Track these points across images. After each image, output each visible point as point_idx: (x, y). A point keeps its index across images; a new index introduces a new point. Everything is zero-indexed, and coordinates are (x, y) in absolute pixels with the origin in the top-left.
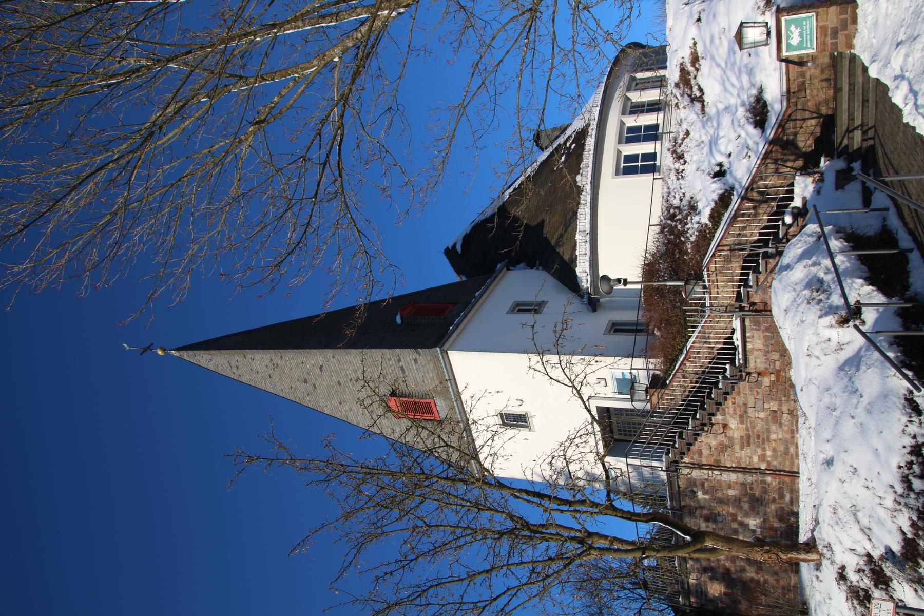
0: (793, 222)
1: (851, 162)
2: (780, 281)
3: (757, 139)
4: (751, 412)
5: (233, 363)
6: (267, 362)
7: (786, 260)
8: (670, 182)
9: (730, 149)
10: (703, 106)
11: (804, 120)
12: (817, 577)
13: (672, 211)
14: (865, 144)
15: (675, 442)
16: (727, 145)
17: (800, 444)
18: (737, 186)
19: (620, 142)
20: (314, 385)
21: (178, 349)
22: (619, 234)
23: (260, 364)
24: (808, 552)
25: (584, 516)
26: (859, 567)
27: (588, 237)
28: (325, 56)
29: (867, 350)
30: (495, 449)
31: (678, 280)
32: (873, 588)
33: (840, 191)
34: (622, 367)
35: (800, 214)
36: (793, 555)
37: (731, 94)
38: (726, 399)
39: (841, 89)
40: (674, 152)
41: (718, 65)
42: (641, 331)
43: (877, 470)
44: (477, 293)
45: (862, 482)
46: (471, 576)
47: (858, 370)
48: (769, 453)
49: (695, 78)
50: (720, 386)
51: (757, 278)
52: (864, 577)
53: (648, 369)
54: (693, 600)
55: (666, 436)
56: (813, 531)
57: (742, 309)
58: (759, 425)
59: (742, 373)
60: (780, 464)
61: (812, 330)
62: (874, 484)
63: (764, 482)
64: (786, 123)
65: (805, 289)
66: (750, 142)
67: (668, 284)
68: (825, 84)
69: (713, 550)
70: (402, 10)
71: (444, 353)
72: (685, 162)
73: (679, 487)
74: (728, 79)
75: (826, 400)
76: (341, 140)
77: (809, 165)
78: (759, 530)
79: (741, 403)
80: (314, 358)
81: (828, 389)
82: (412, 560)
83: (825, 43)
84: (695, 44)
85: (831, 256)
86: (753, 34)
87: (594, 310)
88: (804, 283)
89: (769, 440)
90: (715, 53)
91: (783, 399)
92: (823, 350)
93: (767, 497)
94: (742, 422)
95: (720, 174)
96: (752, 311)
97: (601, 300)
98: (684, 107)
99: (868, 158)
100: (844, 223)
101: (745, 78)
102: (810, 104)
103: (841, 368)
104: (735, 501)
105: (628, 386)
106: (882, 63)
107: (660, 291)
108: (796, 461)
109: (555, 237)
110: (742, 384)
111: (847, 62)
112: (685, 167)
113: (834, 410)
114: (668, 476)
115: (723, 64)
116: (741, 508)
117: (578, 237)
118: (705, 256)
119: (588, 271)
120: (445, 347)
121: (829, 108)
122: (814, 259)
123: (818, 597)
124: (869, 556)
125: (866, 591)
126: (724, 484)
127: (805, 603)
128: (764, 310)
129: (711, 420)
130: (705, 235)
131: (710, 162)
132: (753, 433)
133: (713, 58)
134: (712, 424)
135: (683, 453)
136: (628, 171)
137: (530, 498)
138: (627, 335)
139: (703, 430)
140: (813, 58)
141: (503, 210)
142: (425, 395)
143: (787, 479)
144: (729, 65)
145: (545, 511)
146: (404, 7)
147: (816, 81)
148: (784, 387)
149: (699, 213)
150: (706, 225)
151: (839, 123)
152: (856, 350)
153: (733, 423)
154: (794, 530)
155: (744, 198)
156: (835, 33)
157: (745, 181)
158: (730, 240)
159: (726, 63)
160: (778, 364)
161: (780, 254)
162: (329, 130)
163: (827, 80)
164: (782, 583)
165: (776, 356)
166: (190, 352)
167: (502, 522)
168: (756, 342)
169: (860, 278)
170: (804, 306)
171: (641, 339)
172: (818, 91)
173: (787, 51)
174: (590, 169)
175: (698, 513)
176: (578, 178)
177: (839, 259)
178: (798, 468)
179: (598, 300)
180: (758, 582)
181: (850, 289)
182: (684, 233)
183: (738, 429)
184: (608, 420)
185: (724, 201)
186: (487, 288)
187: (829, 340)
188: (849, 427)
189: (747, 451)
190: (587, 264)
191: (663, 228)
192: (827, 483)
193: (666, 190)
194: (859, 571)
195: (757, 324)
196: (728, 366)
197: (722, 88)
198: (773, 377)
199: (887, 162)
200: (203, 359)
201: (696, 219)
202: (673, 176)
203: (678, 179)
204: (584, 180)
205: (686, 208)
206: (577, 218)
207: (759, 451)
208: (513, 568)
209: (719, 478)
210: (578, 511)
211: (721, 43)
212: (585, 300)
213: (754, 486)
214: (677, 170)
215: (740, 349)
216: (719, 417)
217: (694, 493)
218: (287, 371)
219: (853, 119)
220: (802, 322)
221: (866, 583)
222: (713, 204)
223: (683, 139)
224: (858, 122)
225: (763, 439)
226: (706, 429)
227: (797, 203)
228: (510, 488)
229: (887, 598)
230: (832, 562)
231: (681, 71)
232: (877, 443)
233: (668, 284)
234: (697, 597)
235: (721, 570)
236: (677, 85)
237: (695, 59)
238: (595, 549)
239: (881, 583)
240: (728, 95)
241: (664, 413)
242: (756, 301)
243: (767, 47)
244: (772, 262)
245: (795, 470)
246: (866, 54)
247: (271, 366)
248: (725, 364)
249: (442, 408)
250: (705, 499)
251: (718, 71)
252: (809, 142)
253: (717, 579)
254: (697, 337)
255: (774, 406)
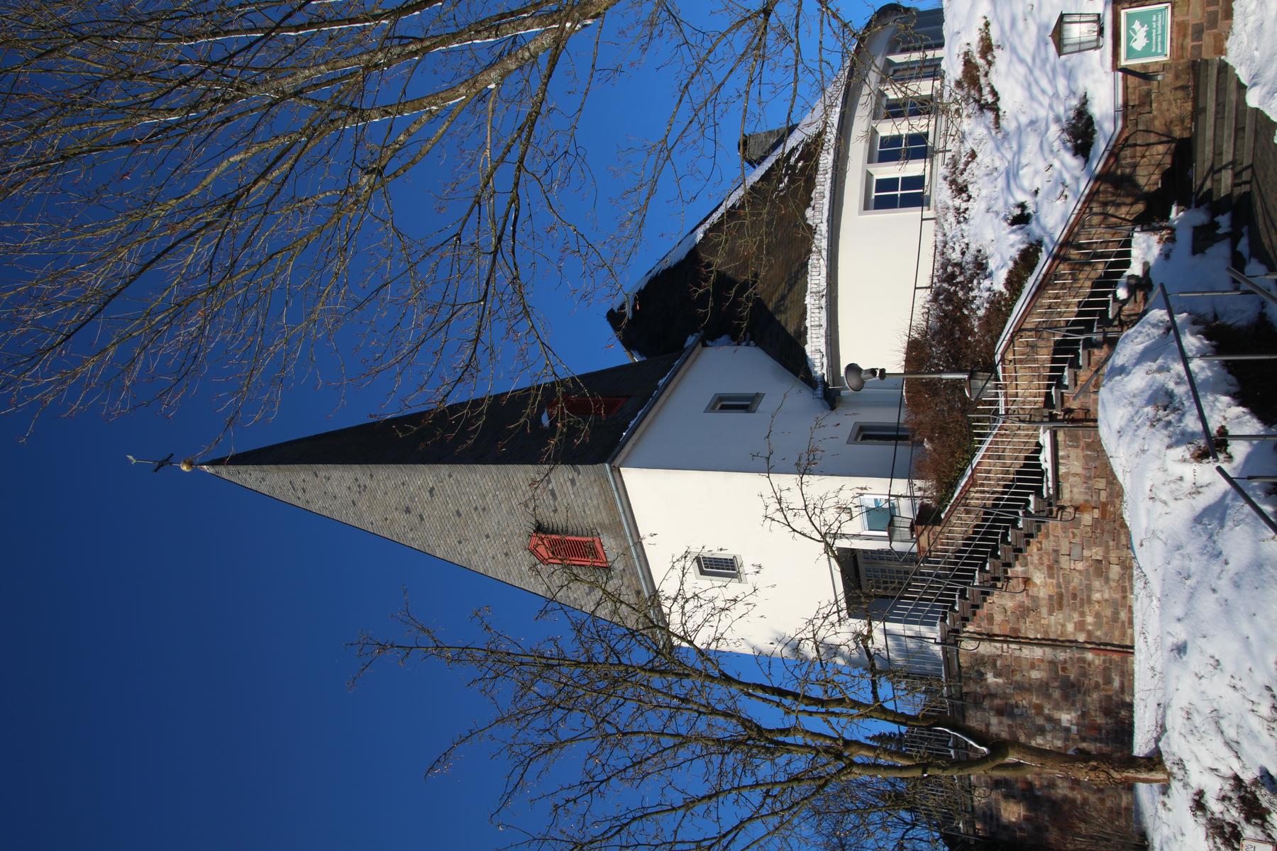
0: (1129, 298)
1: (1217, 215)
2: (1111, 390)
3: (1078, 173)
4: (1065, 562)
5: (298, 484)
6: (349, 482)
7: (1120, 358)
8: (946, 226)
9: (1038, 183)
10: (997, 117)
11: (1148, 145)
12: (1164, 804)
13: (950, 269)
14: (1237, 191)
15: (954, 603)
16: (1029, 179)
17: (1137, 607)
18: (1046, 240)
19: (870, 161)
20: (421, 516)
21: (213, 463)
22: (872, 296)
23: (339, 484)
24: (1151, 770)
25: (843, 720)
26: (1223, 793)
27: (824, 300)
28: (476, 81)
29: (1234, 499)
30: (720, 631)
31: (960, 371)
32: (1243, 823)
33: (1198, 256)
34: (878, 489)
35: (1141, 285)
36: (1131, 774)
37: (1041, 104)
38: (1028, 543)
39: (1204, 110)
40: (953, 182)
41: (1022, 61)
42: (905, 438)
43: (1249, 665)
44: (661, 382)
45: (1227, 679)
46: (689, 804)
47: (1222, 527)
48: (1090, 619)
49: (986, 75)
50: (1020, 525)
51: (1076, 375)
52: (1230, 807)
53: (912, 497)
54: (978, 826)
55: (942, 595)
56: (1157, 740)
57: (1052, 418)
58: (1076, 581)
59: (1052, 506)
60: (1106, 634)
61: (1157, 464)
62: (1244, 684)
63: (1083, 660)
64: (1121, 150)
65: (1147, 404)
66: (1067, 177)
67: (945, 376)
68: (1180, 94)
69: (1017, 766)
70: (589, 22)
71: (616, 470)
72: (970, 197)
73: (959, 666)
74: (1037, 82)
75: (1177, 563)
76: (516, 217)
77: (1152, 218)
78: (1074, 728)
79: (1050, 549)
80: (421, 478)
81: (1179, 548)
82: (602, 782)
83: (1182, 47)
84: (987, 25)
85: (1185, 360)
86: (1077, 32)
87: (833, 408)
88: (1146, 396)
89: (1089, 601)
90: (1016, 42)
91: (1111, 543)
92: (1172, 492)
93: (1086, 682)
94: (1051, 576)
95: (1021, 219)
96: (1069, 421)
97: (843, 393)
98: (969, 116)
99: (1241, 209)
100: (1204, 309)
101: (1062, 84)
102: (1157, 123)
103: (1198, 519)
104: (1041, 686)
105: (883, 517)
106: (1266, 89)
107: (932, 387)
108: (1129, 631)
109: (774, 300)
110: (1051, 523)
111: (1215, 71)
112: (969, 204)
113: (1188, 577)
114: (944, 651)
115: (1029, 60)
116: (1049, 696)
117: (809, 300)
118: (998, 337)
119: (823, 349)
120: (616, 463)
121: (1185, 129)
122: (1160, 361)
123: (1165, 831)
124: (1236, 778)
125: (1234, 826)
126: (1024, 662)
127: (1143, 835)
128: (1086, 421)
129: (1006, 572)
130: (1000, 308)
131: (1006, 203)
132: (1067, 590)
133: (1014, 50)
134: (1009, 578)
135: (965, 620)
136: (883, 204)
137: (767, 696)
138: (880, 444)
139: (994, 586)
140: (1164, 66)
141: (694, 254)
142: (591, 532)
143: (1116, 657)
144: (1038, 62)
145: (787, 713)
146: (593, 17)
147: (1166, 90)
148: (1111, 526)
149: (991, 275)
150: (1001, 293)
151: (1199, 158)
152: (1220, 495)
153: (1038, 578)
154: (1124, 731)
155: (1056, 258)
156: (1198, 32)
157: (1059, 233)
158: (1034, 320)
159: (1034, 59)
160: (1103, 495)
161: (1112, 343)
162: (496, 205)
163: (1183, 88)
164: (1109, 803)
165: (1101, 484)
166: (232, 468)
167: (726, 728)
168: (1073, 464)
169: (1226, 394)
170: (1145, 430)
171: (904, 450)
172: (1170, 104)
173: (1127, 58)
174: (826, 201)
175: (986, 704)
176: (809, 213)
177: (1195, 365)
178: (1132, 640)
179: (838, 392)
180: (1073, 801)
181: (1212, 410)
182: (967, 302)
183: (1045, 585)
184: (852, 565)
185: (1027, 260)
186: (676, 373)
187: (1181, 479)
188: (1207, 605)
189: (1059, 617)
190: (823, 340)
191: (936, 295)
192: (1178, 678)
193: (940, 238)
194: (1224, 799)
195: (1074, 438)
196: (1031, 498)
197: (1027, 94)
198: (1096, 513)
199: (1269, 223)
200: (252, 477)
201: (986, 283)
202: (951, 218)
203: (959, 222)
204: (817, 216)
205: (971, 266)
206: (806, 272)
207: (1076, 616)
208: (745, 792)
209: (1017, 653)
210: (833, 713)
211: (1027, 28)
212: (819, 392)
213: (1068, 666)
214: (957, 209)
215: (1050, 474)
216: (1018, 569)
217: (981, 675)
218: (379, 495)
219: (1221, 154)
220: (1143, 451)
221: (1234, 815)
222: (1011, 264)
223: (967, 163)
224: (1228, 157)
225: (1082, 599)
226: (999, 585)
227: (1136, 269)
228: (740, 683)
229: (1261, 836)
230: (1186, 785)
231: (965, 64)
232: (1246, 628)
233: (945, 376)
234: (985, 823)
235: (1019, 785)
236: (959, 84)
237: (987, 47)
238: (858, 765)
239: (1256, 816)
240: (1035, 105)
241: (938, 563)
242: (1073, 407)
243: (1098, 52)
244: (1099, 354)
245: (1128, 643)
246: (1243, 68)
247: (355, 488)
248: (1028, 494)
249: (610, 545)
250: (997, 685)
251: (1021, 70)
252: (1154, 177)
253: (1014, 797)
254: (988, 450)
255: (1096, 553)
